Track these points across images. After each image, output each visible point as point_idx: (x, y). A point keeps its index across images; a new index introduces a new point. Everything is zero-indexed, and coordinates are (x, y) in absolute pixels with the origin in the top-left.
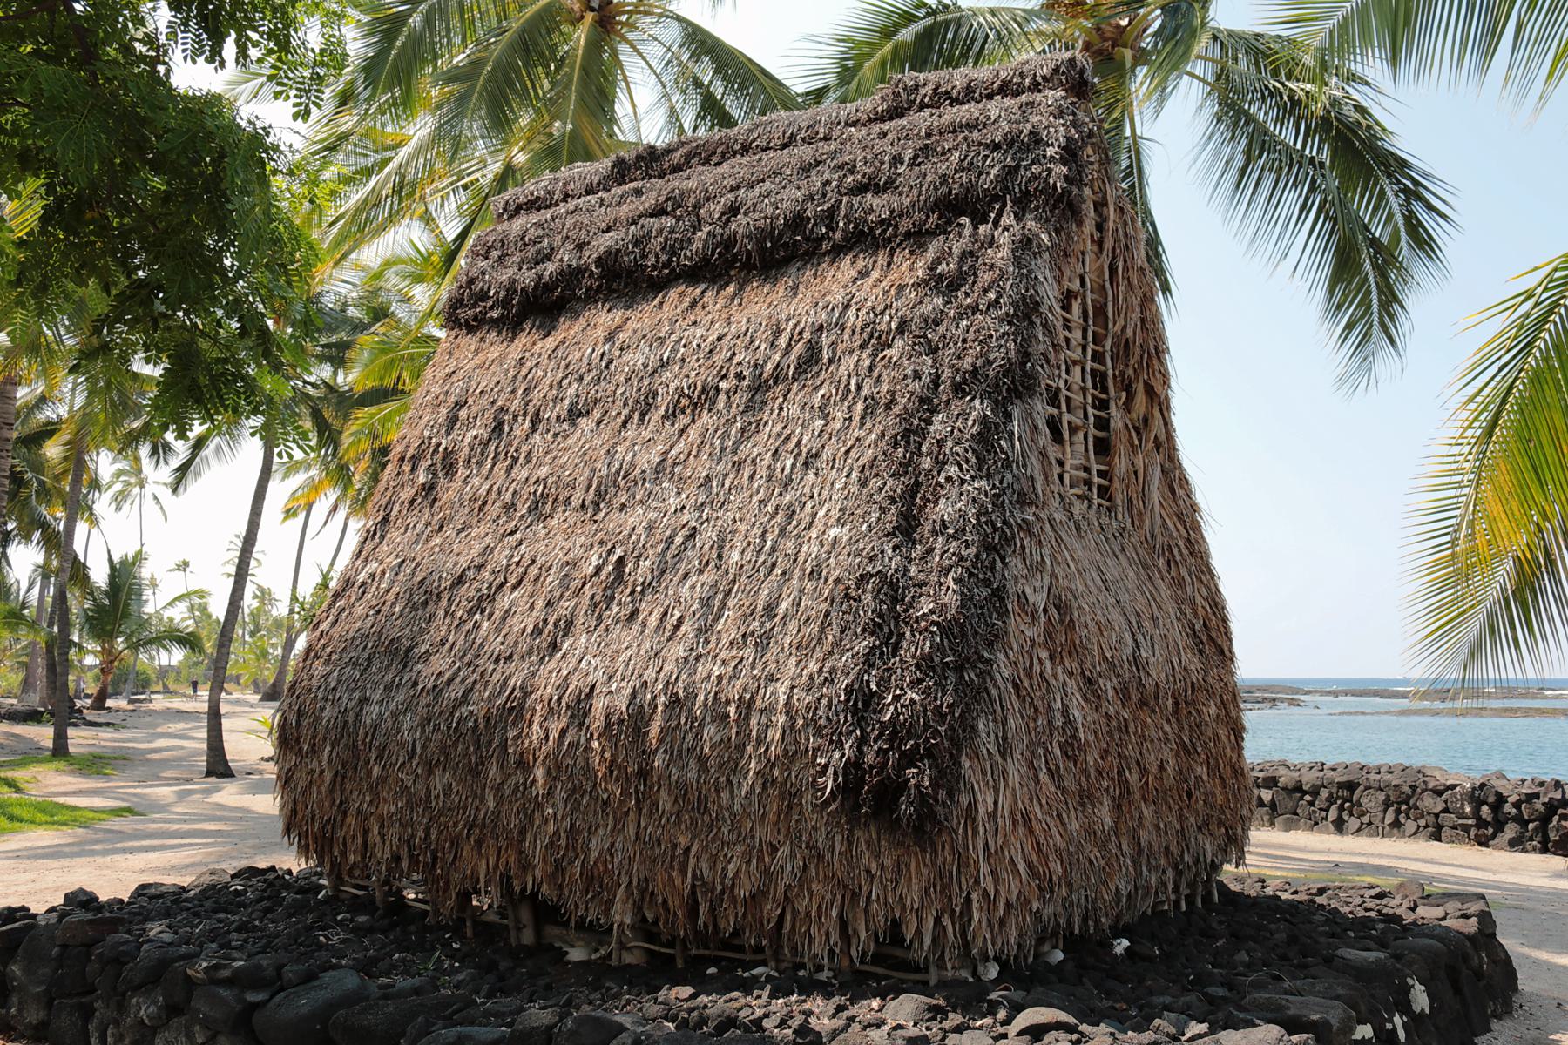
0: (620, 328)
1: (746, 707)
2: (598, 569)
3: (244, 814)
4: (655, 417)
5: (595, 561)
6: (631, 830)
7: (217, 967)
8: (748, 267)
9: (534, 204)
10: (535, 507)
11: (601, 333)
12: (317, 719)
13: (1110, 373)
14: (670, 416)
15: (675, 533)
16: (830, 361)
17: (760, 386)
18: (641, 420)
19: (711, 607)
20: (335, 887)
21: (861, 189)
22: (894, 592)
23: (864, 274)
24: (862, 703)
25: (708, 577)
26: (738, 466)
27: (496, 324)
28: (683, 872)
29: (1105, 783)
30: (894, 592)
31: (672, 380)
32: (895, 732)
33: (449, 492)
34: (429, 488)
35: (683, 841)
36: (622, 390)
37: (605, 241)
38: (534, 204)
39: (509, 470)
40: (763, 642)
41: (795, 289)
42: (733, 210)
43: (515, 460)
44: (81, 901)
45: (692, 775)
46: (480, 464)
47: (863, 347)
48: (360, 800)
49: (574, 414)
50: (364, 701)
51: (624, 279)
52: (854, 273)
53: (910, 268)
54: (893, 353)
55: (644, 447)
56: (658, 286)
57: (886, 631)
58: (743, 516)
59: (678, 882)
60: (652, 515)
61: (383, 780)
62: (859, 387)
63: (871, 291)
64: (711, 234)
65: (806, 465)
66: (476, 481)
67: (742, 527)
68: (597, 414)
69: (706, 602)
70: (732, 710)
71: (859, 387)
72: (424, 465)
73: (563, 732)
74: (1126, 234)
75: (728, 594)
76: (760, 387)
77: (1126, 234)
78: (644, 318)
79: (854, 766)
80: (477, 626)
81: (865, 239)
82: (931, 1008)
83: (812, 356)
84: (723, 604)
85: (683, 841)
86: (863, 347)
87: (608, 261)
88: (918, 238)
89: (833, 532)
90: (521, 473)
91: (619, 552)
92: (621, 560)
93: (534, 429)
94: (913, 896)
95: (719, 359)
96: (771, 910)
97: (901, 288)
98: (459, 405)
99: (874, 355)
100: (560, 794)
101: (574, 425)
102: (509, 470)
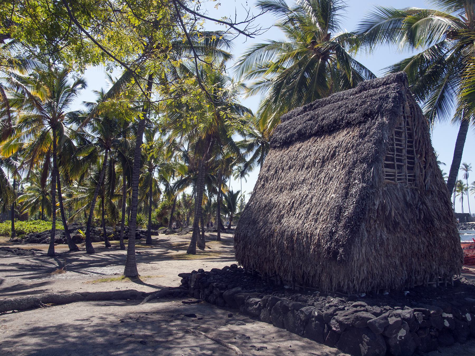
0: (300, 148)
1: (312, 234)
2: (289, 204)
3: (122, 255)
4: (304, 169)
5: (289, 202)
6: (292, 260)
7: (217, 284)
8: (326, 132)
9: (289, 118)
10: (281, 190)
11: (296, 149)
12: (240, 235)
13: (415, 150)
14: (307, 168)
15: (304, 196)
16: (338, 155)
17: (324, 162)
18: (302, 170)
19: (308, 213)
20: (246, 271)
21: (349, 112)
22: (341, 209)
23: (348, 133)
24: (332, 234)
25: (308, 206)
26: (318, 180)
27: (279, 147)
28: (301, 270)
29: (252, 255)
30: (341, 209)
31: (308, 160)
32: (337, 241)
33: (267, 186)
34: (263, 185)
35: (301, 263)
36: (299, 162)
37: (299, 127)
38: (289, 118)
39: (277, 181)
40: (316, 221)
41: (334, 137)
42: (323, 119)
43: (279, 179)
44: (201, 271)
45: (302, 249)
46: (273, 180)
47: (344, 151)
48: (247, 253)
49: (290, 168)
50: (248, 232)
51: (302, 136)
52: (346, 133)
53: (356, 132)
54: (350, 153)
55: (302, 174)
56: (309, 137)
57: (338, 219)
58: (317, 192)
59: (300, 272)
60: (300, 191)
61: (251, 248)
62: (343, 161)
63: (348, 139)
64: (319, 125)
65: (330, 180)
66: (271, 184)
67: (316, 194)
68: (294, 168)
69: (307, 211)
70: (309, 235)
71: (343, 161)
72: (263, 180)
73: (280, 239)
74: (418, 114)
75: (311, 210)
76: (324, 161)
77: (418, 114)
78: (306, 144)
79: (329, 248)
80: (268, 216)
81: (349, 125)
82: (341, 301)
83: (333, 155)
84: (310, 212)
85: (301, 263)
86: (344, 151)
87: (299, 132)
88: (360, 123)
89: (332, 195)
90: (279, 182)
91: (293, 200)
92: (294, 202)
93: (282, 171)
94: (342, 277)
95: (317, 155)
96: (317, 278)
97: (354, 137)
98: (270, 166)
99: (346, 154)
100: (279, 253)
101: (290, 170)
102: (277, 181)
